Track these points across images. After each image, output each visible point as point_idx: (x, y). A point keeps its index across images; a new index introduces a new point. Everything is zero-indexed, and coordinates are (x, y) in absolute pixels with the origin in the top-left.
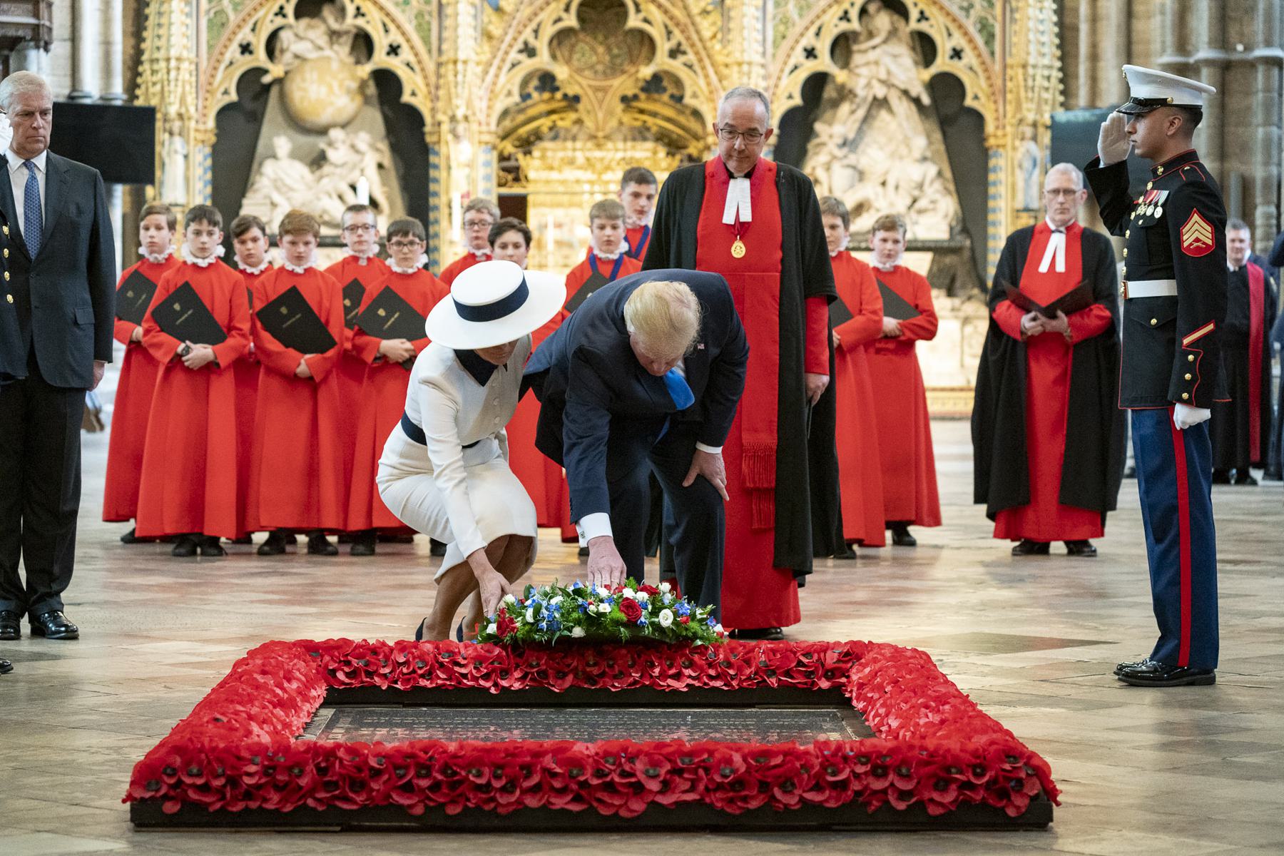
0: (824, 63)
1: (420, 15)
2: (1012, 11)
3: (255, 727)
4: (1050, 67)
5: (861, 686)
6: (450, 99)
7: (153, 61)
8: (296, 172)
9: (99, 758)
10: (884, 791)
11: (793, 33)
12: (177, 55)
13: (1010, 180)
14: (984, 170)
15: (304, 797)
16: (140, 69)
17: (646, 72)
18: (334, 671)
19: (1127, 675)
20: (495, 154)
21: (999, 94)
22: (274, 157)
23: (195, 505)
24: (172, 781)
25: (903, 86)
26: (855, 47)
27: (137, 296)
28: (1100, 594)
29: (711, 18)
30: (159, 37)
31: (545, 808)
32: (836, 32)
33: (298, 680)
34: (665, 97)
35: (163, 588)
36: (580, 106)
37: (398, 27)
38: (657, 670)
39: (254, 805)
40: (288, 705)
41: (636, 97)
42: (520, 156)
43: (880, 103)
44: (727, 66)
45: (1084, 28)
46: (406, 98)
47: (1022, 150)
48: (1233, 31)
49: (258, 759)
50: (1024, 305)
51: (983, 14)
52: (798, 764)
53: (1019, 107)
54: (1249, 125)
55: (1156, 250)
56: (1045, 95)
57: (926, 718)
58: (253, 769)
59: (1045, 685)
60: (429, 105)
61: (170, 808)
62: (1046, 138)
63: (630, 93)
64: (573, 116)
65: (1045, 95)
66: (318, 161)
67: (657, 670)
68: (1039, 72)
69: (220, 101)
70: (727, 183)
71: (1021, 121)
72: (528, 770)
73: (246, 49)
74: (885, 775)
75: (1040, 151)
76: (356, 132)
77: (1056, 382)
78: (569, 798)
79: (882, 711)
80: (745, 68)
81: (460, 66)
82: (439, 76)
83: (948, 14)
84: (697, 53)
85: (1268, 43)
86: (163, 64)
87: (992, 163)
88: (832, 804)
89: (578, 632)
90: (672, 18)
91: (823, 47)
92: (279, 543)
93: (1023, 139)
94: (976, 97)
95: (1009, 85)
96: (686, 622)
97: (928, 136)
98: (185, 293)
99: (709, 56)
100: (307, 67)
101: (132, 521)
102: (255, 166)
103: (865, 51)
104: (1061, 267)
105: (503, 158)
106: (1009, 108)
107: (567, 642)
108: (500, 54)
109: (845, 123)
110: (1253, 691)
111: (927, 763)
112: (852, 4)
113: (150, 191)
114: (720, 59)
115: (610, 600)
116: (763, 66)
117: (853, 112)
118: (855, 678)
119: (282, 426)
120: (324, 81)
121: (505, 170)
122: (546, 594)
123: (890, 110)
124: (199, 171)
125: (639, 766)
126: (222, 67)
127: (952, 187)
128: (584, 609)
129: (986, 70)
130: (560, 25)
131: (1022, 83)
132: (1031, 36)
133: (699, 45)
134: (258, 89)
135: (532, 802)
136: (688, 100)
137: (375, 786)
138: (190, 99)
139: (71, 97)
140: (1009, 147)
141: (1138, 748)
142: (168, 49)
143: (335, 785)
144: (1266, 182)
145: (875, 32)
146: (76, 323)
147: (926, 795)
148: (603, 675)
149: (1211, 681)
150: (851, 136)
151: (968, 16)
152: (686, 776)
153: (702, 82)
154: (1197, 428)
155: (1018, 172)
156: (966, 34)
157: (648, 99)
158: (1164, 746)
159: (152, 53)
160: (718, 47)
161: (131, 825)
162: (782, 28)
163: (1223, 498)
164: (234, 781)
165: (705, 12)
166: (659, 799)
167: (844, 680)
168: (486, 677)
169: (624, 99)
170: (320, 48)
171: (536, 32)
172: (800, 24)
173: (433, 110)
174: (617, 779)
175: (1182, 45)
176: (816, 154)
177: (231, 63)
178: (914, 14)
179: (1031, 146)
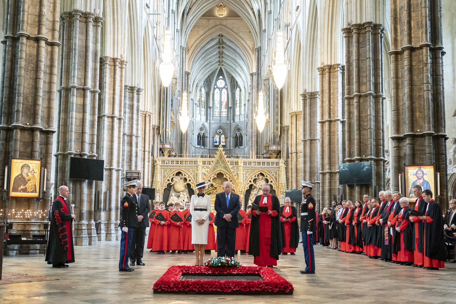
0: (252, 183)
8: (175, 198)
11: (248, 179)
23: (162, 246)
28: (296, 260)
31: (216, 291)
40: (176, 275)
45: (290, 178)
48: (312, 179)
55: (305, 208)
57: (273, 278)
61: (159, 290)
62: (285, 194)
66: (178, 197)
72: (214, 285)
73: (168, 180)
75: (284, 196)
85: (317, 180)
89: (220, 265)
91: (252, 181)
92: (173, 252)
98: (160, 214)
104: (288, 211)
107: (218, 266)
111: (273, 284)
119: (175, 233)
120: (180, 185)
125: (230, 284)
135: (214, 290)
144: (317, 200)
149: (314, 273)
154: (311, 234)
158: (308, 283)
163: (314, 246)
164: (169, 286)
172: (249, 177)
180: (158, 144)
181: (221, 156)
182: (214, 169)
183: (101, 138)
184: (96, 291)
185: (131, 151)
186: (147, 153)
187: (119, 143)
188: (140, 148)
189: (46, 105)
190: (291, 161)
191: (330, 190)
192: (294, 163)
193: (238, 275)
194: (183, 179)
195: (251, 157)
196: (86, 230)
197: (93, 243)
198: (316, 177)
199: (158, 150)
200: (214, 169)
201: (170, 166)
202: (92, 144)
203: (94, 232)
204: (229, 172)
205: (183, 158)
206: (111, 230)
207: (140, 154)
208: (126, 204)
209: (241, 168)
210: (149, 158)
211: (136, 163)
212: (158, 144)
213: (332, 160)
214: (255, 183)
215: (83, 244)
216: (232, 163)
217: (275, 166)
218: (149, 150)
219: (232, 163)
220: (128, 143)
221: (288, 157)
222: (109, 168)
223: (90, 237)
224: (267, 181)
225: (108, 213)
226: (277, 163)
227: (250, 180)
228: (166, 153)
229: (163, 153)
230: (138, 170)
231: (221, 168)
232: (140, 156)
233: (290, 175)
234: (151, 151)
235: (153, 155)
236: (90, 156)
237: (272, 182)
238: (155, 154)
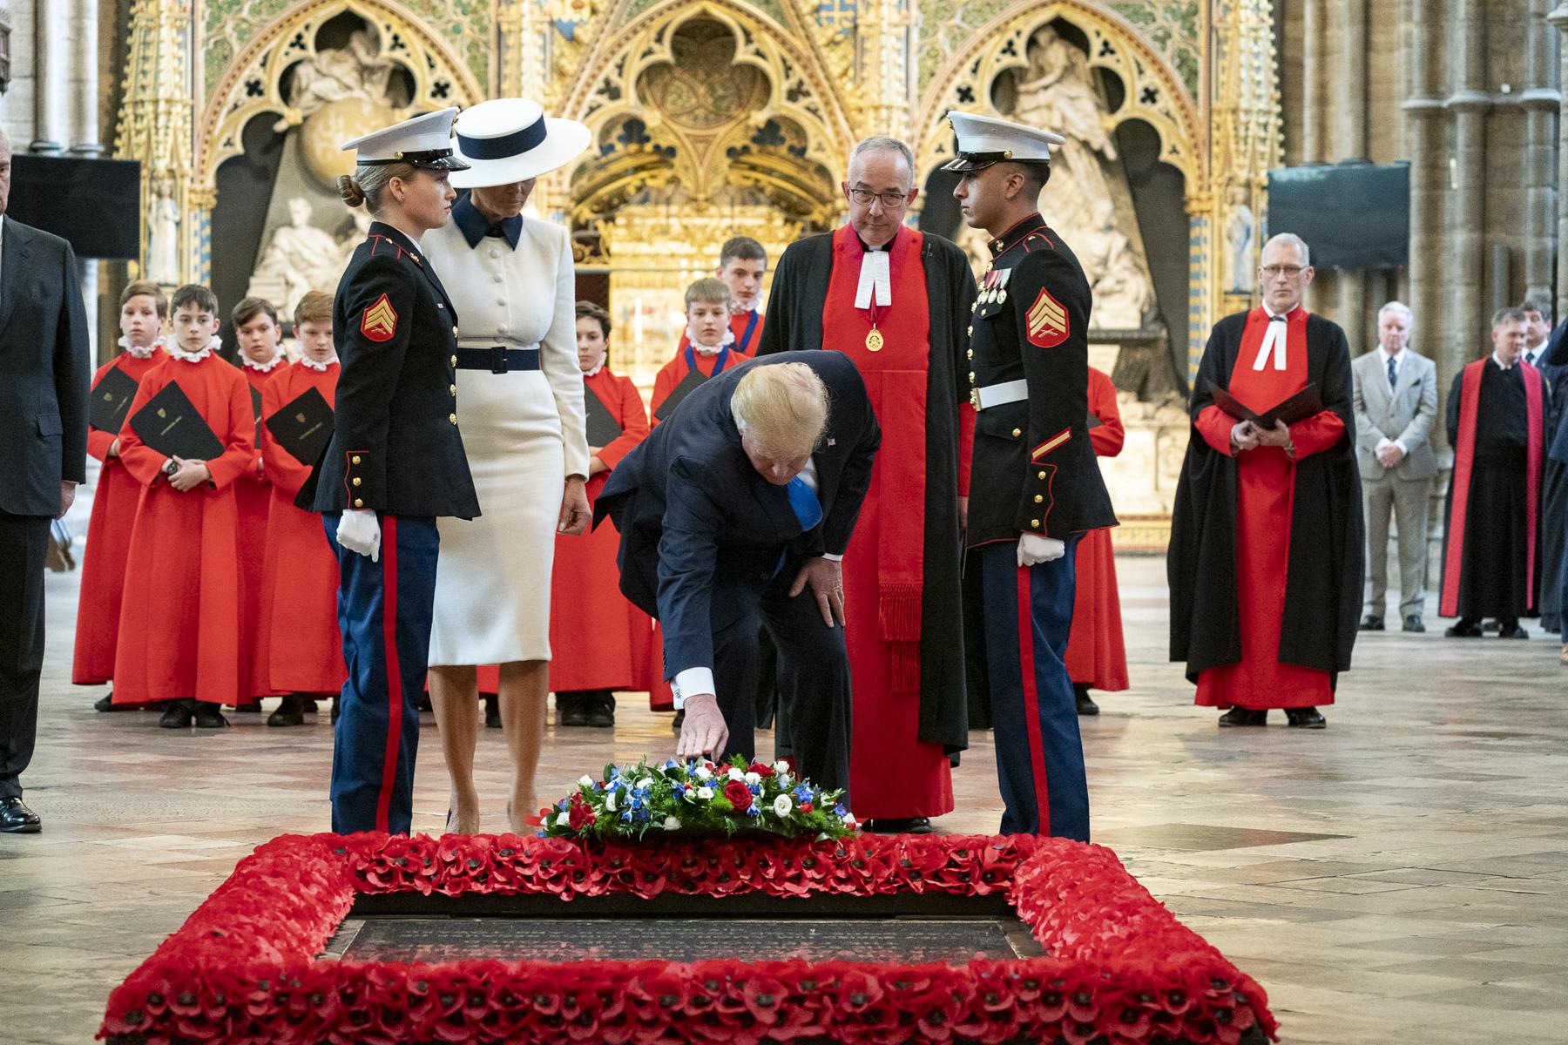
1: (473, 46)
4: (1268, 113)
5: (1028, 891)
7: (136, 103)
9: (66, 983)
10: (1057, 1024)
12: (167, 96)
13: (1217, 254)
14: (1185, 242)
15: (326, 1031)
16: (121, 113)
17: (759, 118)
18: (364, 873)
21: (1204, 146)
22: (290, 224)
23: (186, 663)
24: (158, 1012)
25: (1081, 137)
26: (1022, 88)
27: (117, 400)
28: (1329, 775)
29: (840, 51)
30: (144, 73)
33: (319, 883)
34: (783, 150)
35: (147, 767)
36: (676, 161)
38: (771, 872)
40: (305, 915)
41: (746, 150)
42: (600, 224)
44: (860, 110)
45: (1310, 64)
47: (1232, 217)
48: (1497, 68)
49: (267, 984)
50: (1235, 412)
51: (1183, 46)
52: (948, 990)
53: (1228, 162)
54: (1516, 185)
56: (1261, 148)
58: (260, 996)
62: (1262, 201)
63: (738, 145)
65: (1261, 148)
67: (771, 872)
68: (1253, 118)
69: (221, 154)
70: (861, 258)
72: (609, 997)
73: (254, 88)
74: (1058, 1004)
75: (1255, 219)
77: (1276, 508)
78: (660, 1032)
80: (884, 113)
84: (822, 94)
85: (1541, 84)
86: (149, 108)
87: (1194, 233)
89: (672, 823)
93: (1233, 203)
94: (1174, 151)
95: (1215, 134)
96: (808, 811)
97: (1114, 200)
98: (172, 396)
100: (332, 111)
101: (110, 684)
104: (1280, 364)
105: (578, 226)
106: (1214, 163)
107: (658, 836)
108: (575, 96)
111: (1106, 988)
112: (1018, 33)
113: (132, 267)
114: (852, 101)
115: (712, 784)
116: (906, 110)
118: (1020, 881)
122: (631, 776)
123: (1066, 167)
125: (749, 992)
126: (225, 111)
127: (1143, 263)
128: (679, 793)
131: (1232, 133)
132: (1244, 74)
133: (825, 83)
134: (269, 139)
136: (811, 153)
137: (415, 1018)
138: (184, 152)
139: (33, 149)
140: (1216, 214)
142: (156, 89)
143: (365, 1016)
144: (1539, 256)
145: (1047, 68)
146: (39, 435)
147: (1111, 1029)
148: (703, 877)
151: (1163, 49)
152: (808, 1004)
153: (829, 131)
155: (1226, 243)
159: (135, 92)
160: (849, 86)
162: (930, 63)
164: (237, 1012)
165: (833, 43)
166: (775, 1034)
167: (1007, 884)
168: (556, 880)
169: (731, 152)
170: (348, 88)
172: (953, 58)
174: (721, 1009)
175: (1433, 86)
177: (236, 106)
178: (1096, 46)
179: (1244, 210)
189: (1332, 32)
193: (824, 907)
194: (381, 80)
198: (1529, 60)
204: (779, 15)
227: (963, 78)
233: (1310, 40)
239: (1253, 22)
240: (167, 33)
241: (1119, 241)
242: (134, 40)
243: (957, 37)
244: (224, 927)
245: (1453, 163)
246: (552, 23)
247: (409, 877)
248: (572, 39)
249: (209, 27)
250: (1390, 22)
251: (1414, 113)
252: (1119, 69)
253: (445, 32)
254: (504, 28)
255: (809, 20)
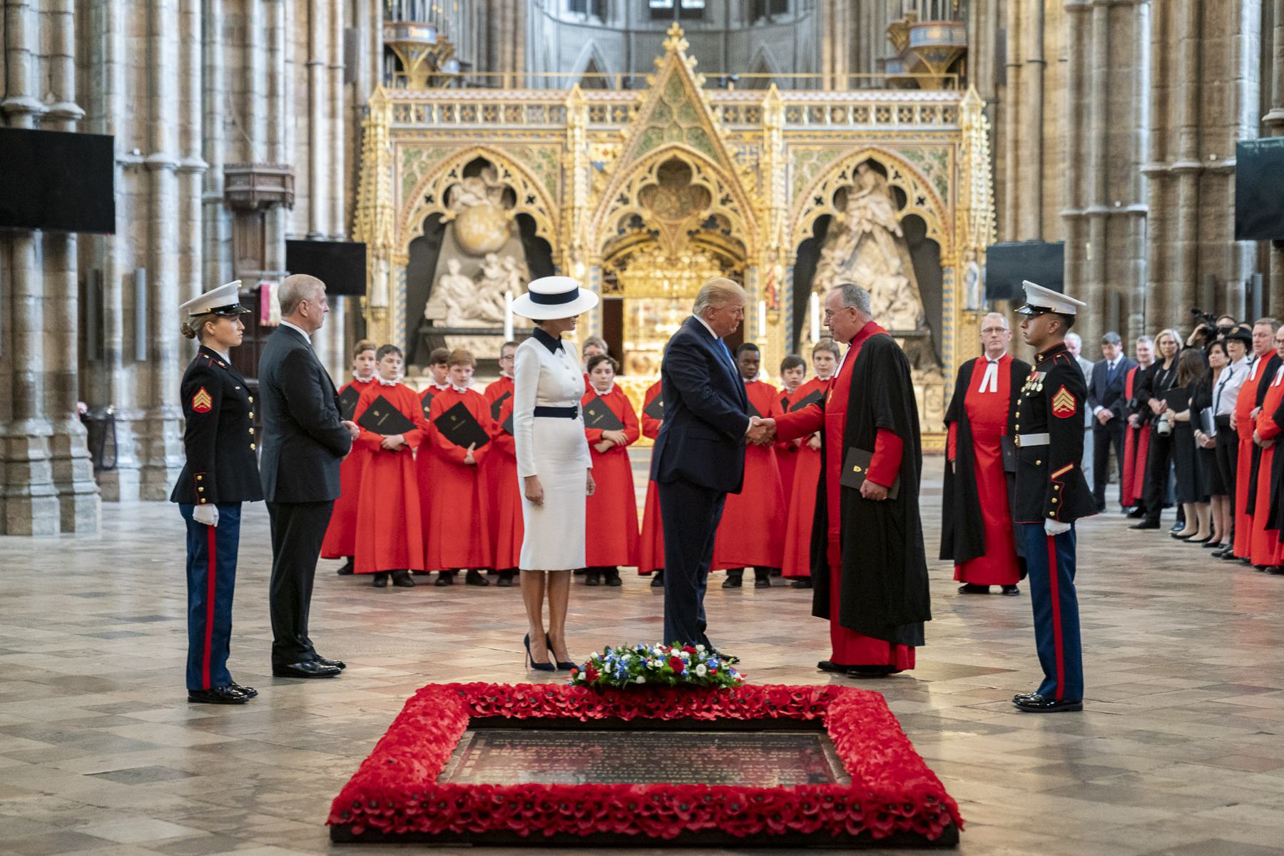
0: (829, 207)
1: (549, 175)
2: (960, 171)
3: (416, 765)
4: (987, 210)
5: (834, 721)
6: (569, 234)
9: (313, 777)
10: (843, 822)
11: (807, 187)
14: (940, 281)
17: (705, 214)
18: (474, 705)
19: (1021, 704)
20: (600, 272)
21: (951, 228)
22: (449, 273)
24: (358, 812)
25: (883, 223)
29: (750, 177)
32: (837, 186)
33: (448, 717)
34: (718, 232)
35: (364, 617)
36: (660, 238)
37: (534, 184)
38: (695, 706)
39: (412, 829)
41: (698, 231)
42: (618, 272)
43: (868, 235)
45: (1009, 186)
46: (539, 233)
47: (966, 268)
48: (1113, 193)
53: (964, 238)
58: (413, 803)
59: (964, 710)
60: (555, 237)
61: (357, 830)
63: (694, 228)
64: (654, 244)
66: (479, 276)
67: (695, 706)
69: (412, 235)
71: (966, 248)
72: (599, 806)
73: (429, 199)
76: (505, 256)
79: (847, 745)
80: (774, 212)
81: (576, 212)
82: (562, 218)
83: (915, 174)
84: (740, 202)
86: (372, 211)
87: (945, 276)
88: (807, 831)
89: (641, 680)
90: (723, 177)
91: (828, 196)
92: (447, 577)
94: (934, 231)
95: (958, 223)
97: (901, 258)
98: (381, 404)
99: (749, 204)
100: (471, 211)
102: (435, 280)
103: (857, 199)
105: (606, 273)
108: (604, 203)
109: (842, 249)
110: (1109, 717)
113: (363, 299)
114: (756, 205)
115: (662, 658)
117: (848, 242)
118: (830, 713)
120: (484, 223)
121: (609, 282)
122: (618, 653)
123: (874, 240)
124: (397, 284)
125: (675, 803)
126: (413, 212)
127: (917, 293)
128: (644, 663)
129: (941, 212)
130: (646, 182)
133: (741, 196)
136: (734, 234)
137: (496, 816)
138: (391, 234)
139: (308, 236)
141: (1024, 771)
148: (658, 708)
149: (1080, 709)
150: (847, 258)
153: (743, 221)
155: (964, 284)
156: (927, 187)
157: (707, 232)
160: (754, 197)
161: (328, 839)
162: (799, 184)
164: (400, 812)
165: (746, 173)
167: (823, 713)
168: (577, 710)
169: (690, 233)
170: (479, 199)
171: (629, 187)
172: (812, 181)
173: (558, 242)
175: (1077, 202)
176: (823, 271)
178: (891, 173)
179: (974, 266)
180: (374, 26)
181: (678, 82)
182: (647, 143)
183: (99, 18)
184: (79, 829)
185: (243, 72)
186: (321, 74)
187: (185, 40)
188: (288, 48)
190: (1017, 103)
191: (1196, 257)
192: (1028, 113)
194: (499, 194)
195: (827, 85)
196: (47, 465)
197: (79, 520)
199: (374, 53)
200: (647, 143)
201: (437, 132)
202: (53, 56)
203: (82, 467)
204: (716, 158)
205: (496, 93)
206: (162, 452)
207: (289, 76)
208: (203, 399)
209: (776, 137)
210: (333, 98)
211: (272, 125)
212: (374, 26)
213: (1206, 108)
214: (843, 208)
215: (35, 528)
216: (731, 114)
217: (937, 123)
218: (333, 57)
219: (731, 115)
220: (228, 32)
221: (1000, 81)
222: (140, 160)
223: (67, 497)
224: (899, 197)
225: (145, 372)
226: (950, 113)
227: (817, 192)
228: (415, 66)
229: (399, 66)
230: (281, 161)
231: (680, 138)
232: (291, 87)
233: (1009, 173)
234: (340, 61)
235: (351, 77)
236: (47, 117)
237: (921, 201)
238: (364, 76)
239: (979, 160)
240: (381, 169)
241: (904, 282)
242: (363, 174)
243: (814, 169)
244: (394, 756)
245: (1088, 246)
246: (592, 163)
247: (499, 708)
248: (602, 172)
249: (405, 165)
250: (1054, 163)
251: (1067, 218)
252: (904, 187)
253: (533, 168)
254: (565, 166)
255: (732, 160)
